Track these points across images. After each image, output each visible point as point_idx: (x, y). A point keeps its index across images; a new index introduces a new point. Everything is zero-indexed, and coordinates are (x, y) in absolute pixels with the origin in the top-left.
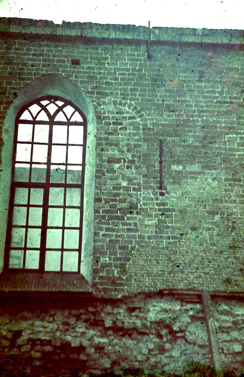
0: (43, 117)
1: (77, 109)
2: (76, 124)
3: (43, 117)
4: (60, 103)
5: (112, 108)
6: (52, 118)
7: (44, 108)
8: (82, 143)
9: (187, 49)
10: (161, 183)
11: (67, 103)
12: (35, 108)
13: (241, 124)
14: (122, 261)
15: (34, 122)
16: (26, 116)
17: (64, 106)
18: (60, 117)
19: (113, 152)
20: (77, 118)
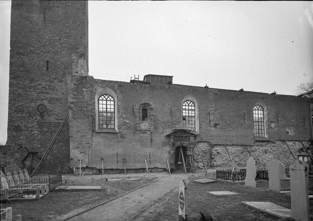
0: (105, 99)
1: (112, 97)
2: (187, 106)
3: (105, 99)
4: (108, 96)
5: (269, 108)
6: (106, 99)
7: (105, 97)
8: (100, 105)
9: (234, 147)
10: (278, 122)
11: (110, 96)
12: (103, 97)
13: (93, 125)
14: (24, 114)
15: (102, 100)
16: (101, 99)
17: (109, 96)
18: (108, 99)
19: (270, 116)
20: (112, 99)
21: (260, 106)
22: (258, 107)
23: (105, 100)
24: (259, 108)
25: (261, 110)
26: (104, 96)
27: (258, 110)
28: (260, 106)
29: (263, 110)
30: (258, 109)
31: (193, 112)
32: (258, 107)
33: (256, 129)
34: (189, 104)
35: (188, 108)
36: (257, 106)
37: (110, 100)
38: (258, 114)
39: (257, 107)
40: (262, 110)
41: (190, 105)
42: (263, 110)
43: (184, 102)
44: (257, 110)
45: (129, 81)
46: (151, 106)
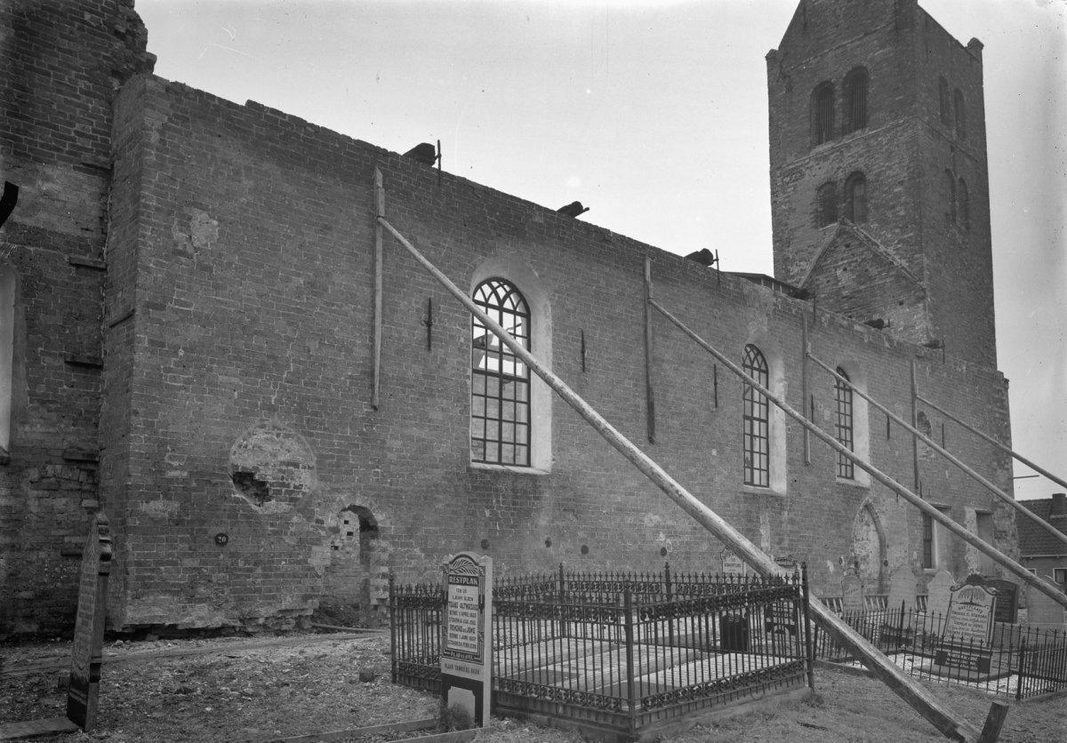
21: (514, 289)
22: (501, 292)
23: (511, 308)
24: (508, 300)
25: (514, 312)
26: (491, 286)
27: (500, 308)
28: (514, 289)
29: (527, 316)
30: (501, 302)
31: (451, 581)
32: (501, 292)
33: (762, 472)
34: (501, 302)
35: (504, 362)
36: (495, 284)
37: (483, 300)
38: (500, 442)
39: (494, 291)
40: (520, 314)
41: (508, 305)
42: (527, 316)
43: (479, 287)
44: (493, 307)
45: (1051, 497)
46: (864, 219)
